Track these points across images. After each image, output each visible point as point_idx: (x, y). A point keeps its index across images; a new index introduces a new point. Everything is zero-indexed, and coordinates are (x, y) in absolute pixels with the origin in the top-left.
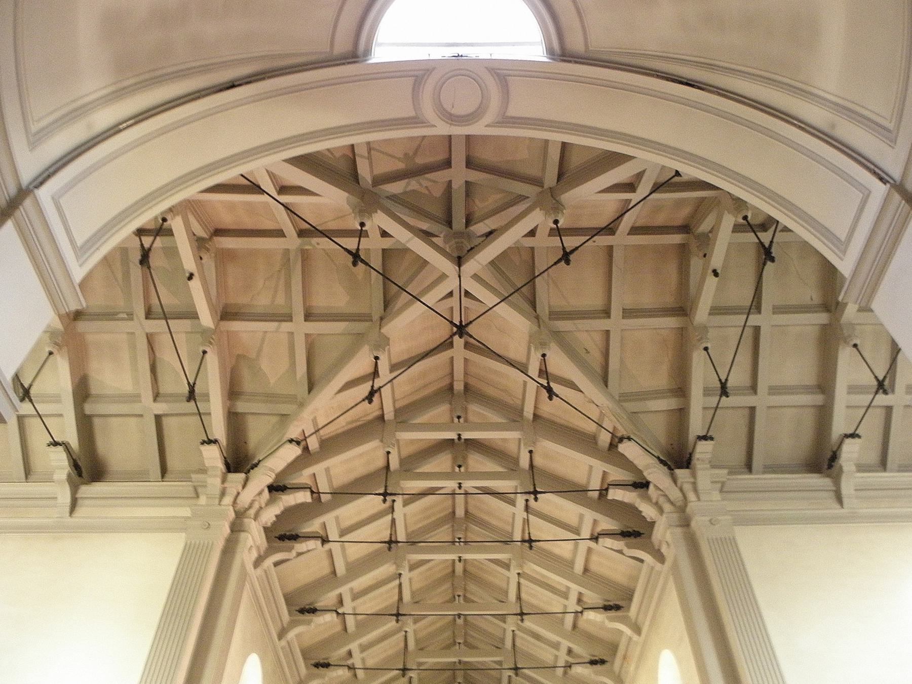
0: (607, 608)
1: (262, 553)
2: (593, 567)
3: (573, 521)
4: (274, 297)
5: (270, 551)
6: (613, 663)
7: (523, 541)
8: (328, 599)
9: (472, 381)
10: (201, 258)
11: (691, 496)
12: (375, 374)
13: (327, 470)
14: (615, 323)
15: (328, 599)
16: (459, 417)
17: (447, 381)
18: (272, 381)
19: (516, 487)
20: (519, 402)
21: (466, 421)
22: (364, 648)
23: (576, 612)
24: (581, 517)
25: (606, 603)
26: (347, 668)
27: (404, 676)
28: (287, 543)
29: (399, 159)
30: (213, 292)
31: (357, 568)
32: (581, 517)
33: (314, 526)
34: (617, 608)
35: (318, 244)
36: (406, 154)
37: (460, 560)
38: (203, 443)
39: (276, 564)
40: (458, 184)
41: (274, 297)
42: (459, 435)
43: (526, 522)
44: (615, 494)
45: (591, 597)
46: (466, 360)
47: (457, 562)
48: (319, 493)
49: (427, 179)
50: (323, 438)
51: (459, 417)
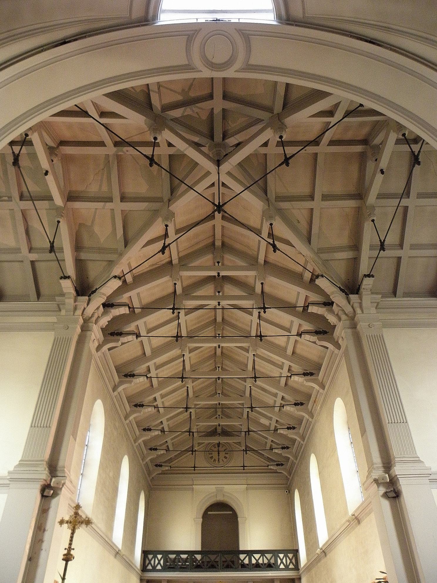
0: (305, 374)
1: (101, 343)
2: (298, 351)
3: (287, 325)
4: (100, 186)
5: (105, 342)
6: (318, 375)
7: (257, 336)
8: (142, 369)
9: (226, 240)
10: (52, 161)
11: (358, 311)
12: (166, 235)
13: (138, 294)
14: (317, 204)
15: (142, 369)
16: (218, 262)
17: (211, 240)
18: (102, 240)
19: (253, 304)
20: (256, 253)
21: (223, 265)
22: (163, 396)
23: (287, 377)
24: (292, 322)
25: (305, 372)
26: (135, 335)
27: (186, 411)
28: (116, 337)
29: (179, 93)
30: (62, 184)
31: (157, 352)
32: (292, 322)
33: (131, 327)
34: (312, 374)
35: (127, 151)
36: (183, 90)
37: (219, 347)
38: (61, 278)
39: (110, 349)
40: (217, 111)
41: (100, 186)
42: (219, 273)
43: (259, 325)
44: (312, 309)
45: (296, 368)
46: (223, 227)
47: (217, 348)
48: (134, 308)
49: (197, 107)
50: (135, 275)
51: (218, 262)
